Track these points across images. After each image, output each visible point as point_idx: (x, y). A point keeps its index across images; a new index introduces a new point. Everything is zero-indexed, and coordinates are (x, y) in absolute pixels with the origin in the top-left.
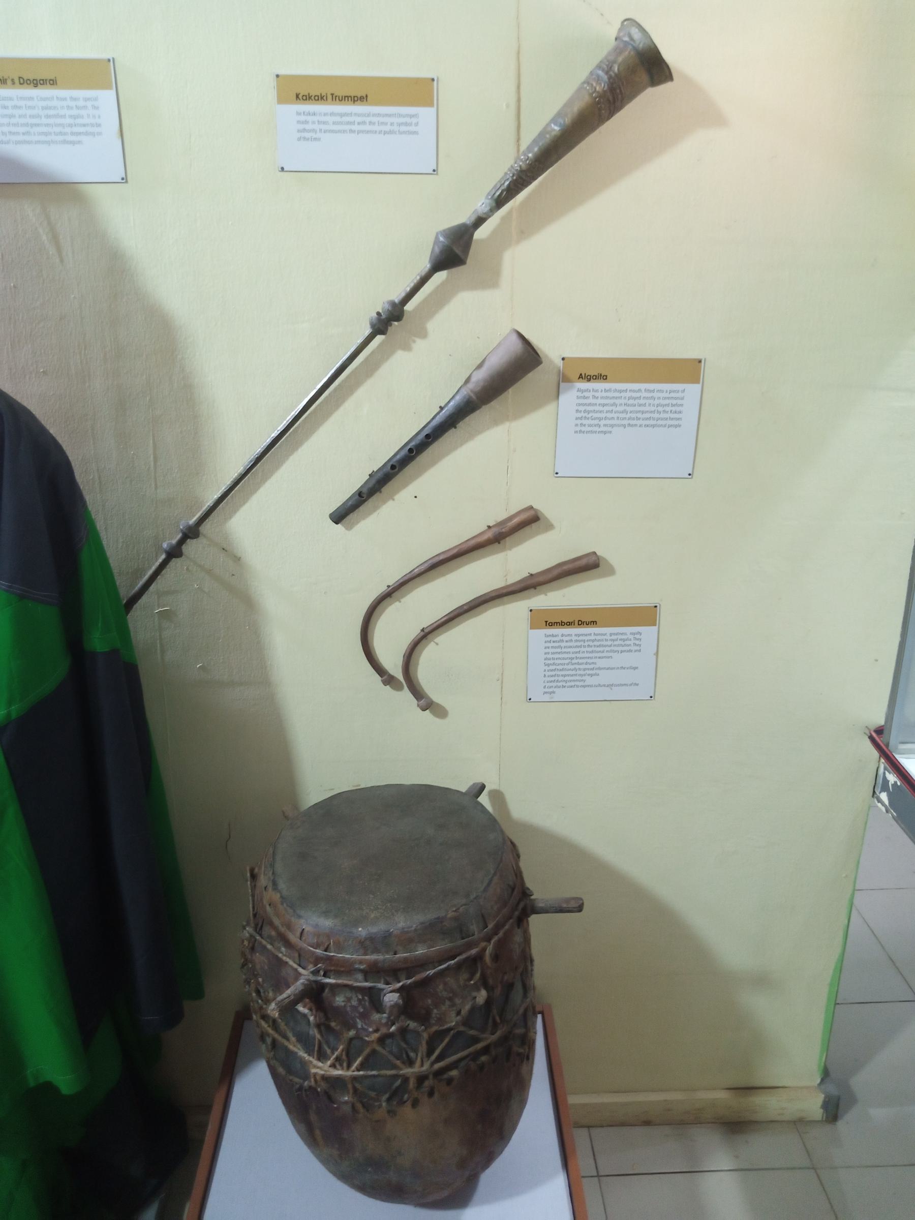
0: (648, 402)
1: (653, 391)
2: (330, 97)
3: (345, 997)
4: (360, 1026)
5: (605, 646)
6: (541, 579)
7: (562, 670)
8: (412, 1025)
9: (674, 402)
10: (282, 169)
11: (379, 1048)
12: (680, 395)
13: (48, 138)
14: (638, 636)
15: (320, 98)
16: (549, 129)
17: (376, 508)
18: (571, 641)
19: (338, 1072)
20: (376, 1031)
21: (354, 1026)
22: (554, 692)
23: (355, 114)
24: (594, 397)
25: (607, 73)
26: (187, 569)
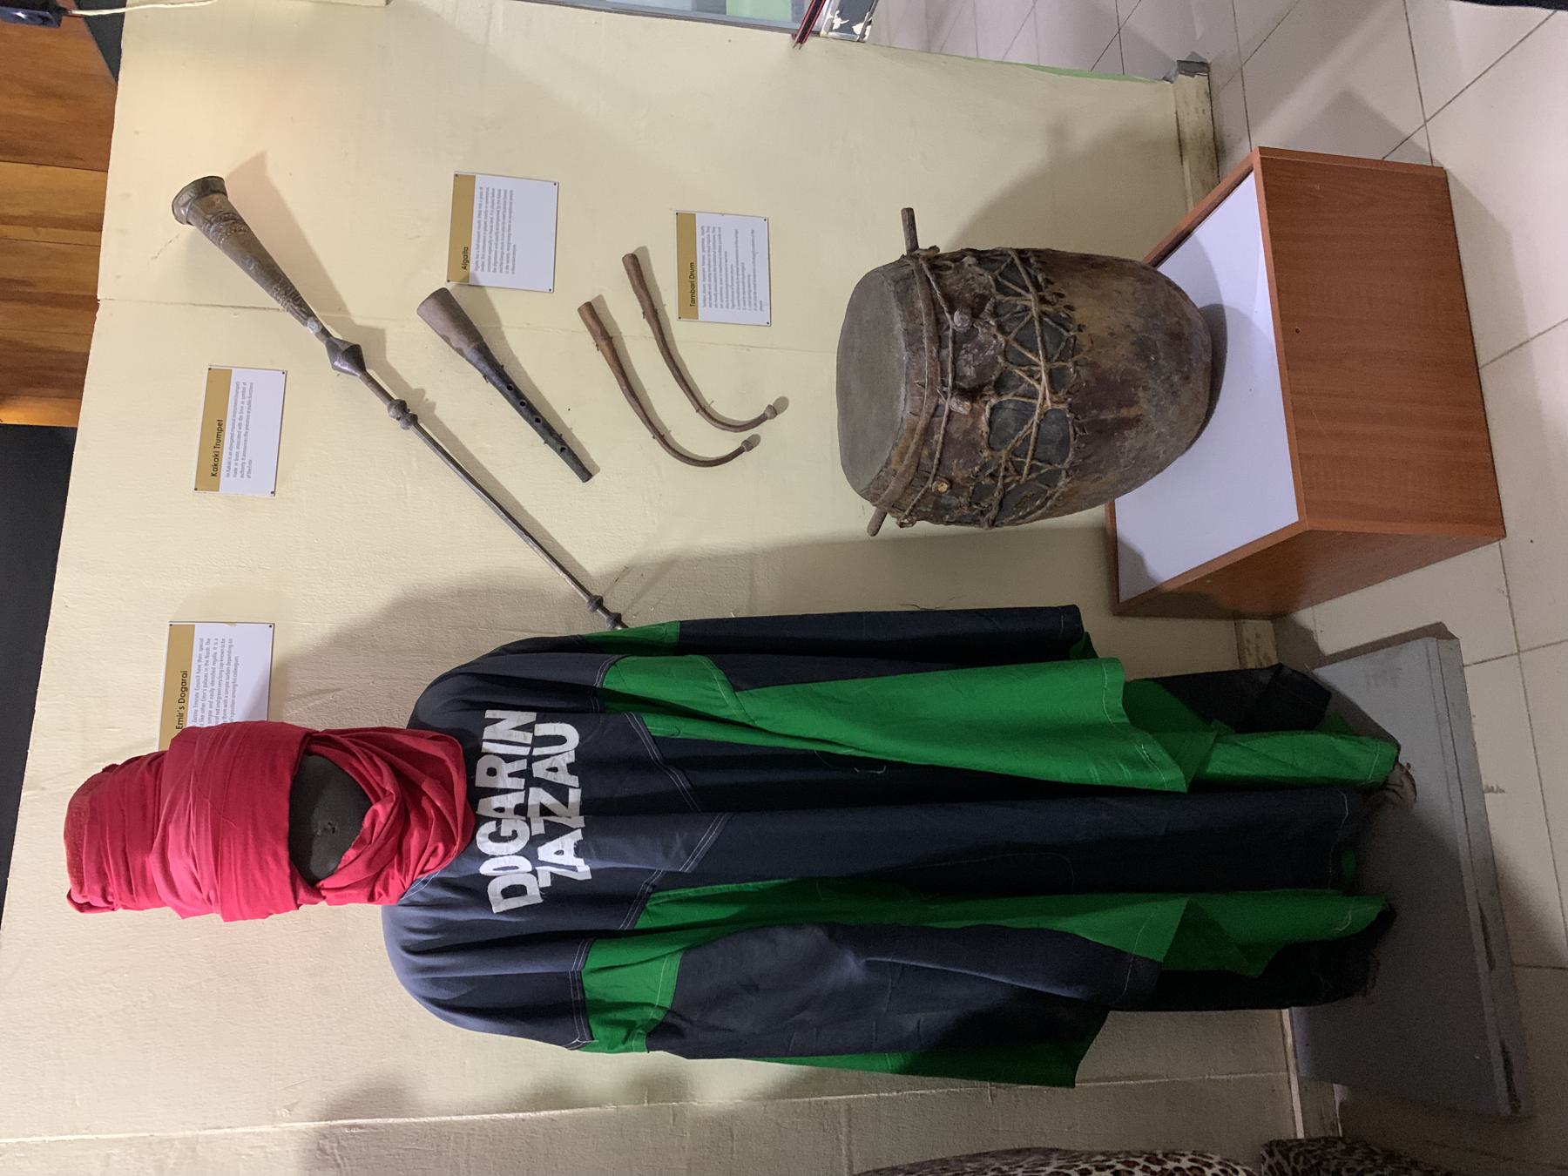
0: (489, 216)
1: (480, 212)
2: (217, 450)
3: (965, 366)
4: (993, 352)
5: (715, 256)
6: (647, 303)
7: (738, 293)
8: (988, 307)
9: (490, 195)
10: (272, 493)
11: (1012, 335)
12: (484, 191)
13: (231, 685)
14: (706, 229)
15: (217, 457)
16: (253, 272)
17: (579, 444)
18: (710, 285)
19: (1044, 378)
20: (995, 337)
21: (994, 358)
22: (761, 302)
23: (232, 430)
24: (483, 257)
25: (212, 224)
26: (635, 615)
